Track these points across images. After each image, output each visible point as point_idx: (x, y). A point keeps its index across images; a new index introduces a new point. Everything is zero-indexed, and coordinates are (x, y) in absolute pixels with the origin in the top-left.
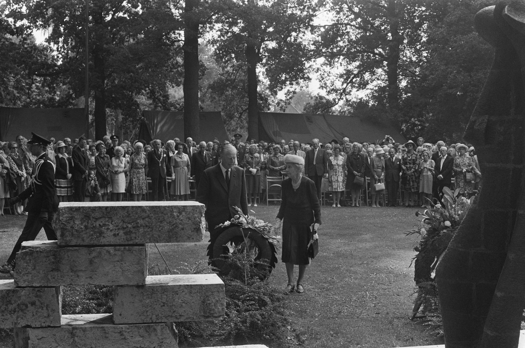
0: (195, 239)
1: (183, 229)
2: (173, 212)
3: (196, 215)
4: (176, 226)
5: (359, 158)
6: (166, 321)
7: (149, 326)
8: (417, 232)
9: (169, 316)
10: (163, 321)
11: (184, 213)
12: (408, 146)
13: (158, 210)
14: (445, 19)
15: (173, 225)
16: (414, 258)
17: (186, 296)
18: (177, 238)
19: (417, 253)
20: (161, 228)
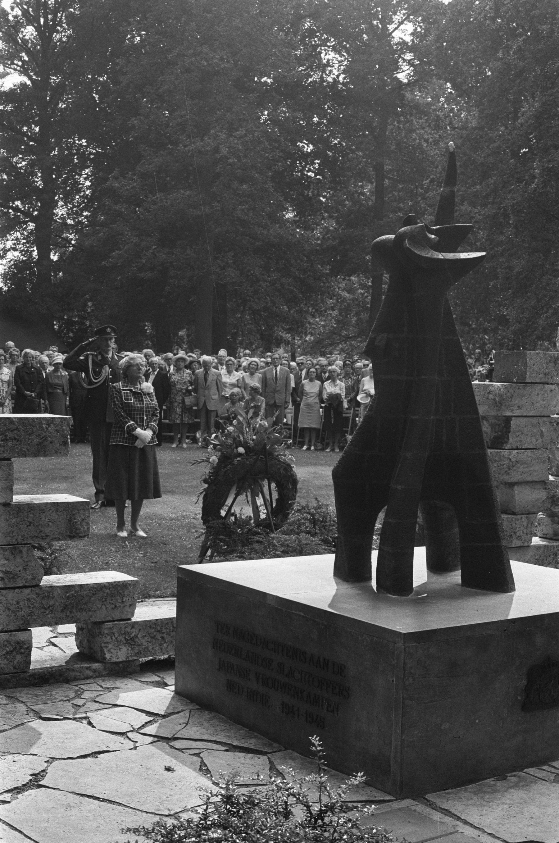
1: (51, 442)
2: (42, 424)
3: (64, 428)
4: (46, 439)
5: (33, 373)
6: (31, 542)
7: (15, 548)
8: (206, 461)
9: (35, 536)
11: (52, 426)
15: (43, 438)
16: (201, 493)
18: (45, 452)
19: (206, 486)
20: (30, 441)
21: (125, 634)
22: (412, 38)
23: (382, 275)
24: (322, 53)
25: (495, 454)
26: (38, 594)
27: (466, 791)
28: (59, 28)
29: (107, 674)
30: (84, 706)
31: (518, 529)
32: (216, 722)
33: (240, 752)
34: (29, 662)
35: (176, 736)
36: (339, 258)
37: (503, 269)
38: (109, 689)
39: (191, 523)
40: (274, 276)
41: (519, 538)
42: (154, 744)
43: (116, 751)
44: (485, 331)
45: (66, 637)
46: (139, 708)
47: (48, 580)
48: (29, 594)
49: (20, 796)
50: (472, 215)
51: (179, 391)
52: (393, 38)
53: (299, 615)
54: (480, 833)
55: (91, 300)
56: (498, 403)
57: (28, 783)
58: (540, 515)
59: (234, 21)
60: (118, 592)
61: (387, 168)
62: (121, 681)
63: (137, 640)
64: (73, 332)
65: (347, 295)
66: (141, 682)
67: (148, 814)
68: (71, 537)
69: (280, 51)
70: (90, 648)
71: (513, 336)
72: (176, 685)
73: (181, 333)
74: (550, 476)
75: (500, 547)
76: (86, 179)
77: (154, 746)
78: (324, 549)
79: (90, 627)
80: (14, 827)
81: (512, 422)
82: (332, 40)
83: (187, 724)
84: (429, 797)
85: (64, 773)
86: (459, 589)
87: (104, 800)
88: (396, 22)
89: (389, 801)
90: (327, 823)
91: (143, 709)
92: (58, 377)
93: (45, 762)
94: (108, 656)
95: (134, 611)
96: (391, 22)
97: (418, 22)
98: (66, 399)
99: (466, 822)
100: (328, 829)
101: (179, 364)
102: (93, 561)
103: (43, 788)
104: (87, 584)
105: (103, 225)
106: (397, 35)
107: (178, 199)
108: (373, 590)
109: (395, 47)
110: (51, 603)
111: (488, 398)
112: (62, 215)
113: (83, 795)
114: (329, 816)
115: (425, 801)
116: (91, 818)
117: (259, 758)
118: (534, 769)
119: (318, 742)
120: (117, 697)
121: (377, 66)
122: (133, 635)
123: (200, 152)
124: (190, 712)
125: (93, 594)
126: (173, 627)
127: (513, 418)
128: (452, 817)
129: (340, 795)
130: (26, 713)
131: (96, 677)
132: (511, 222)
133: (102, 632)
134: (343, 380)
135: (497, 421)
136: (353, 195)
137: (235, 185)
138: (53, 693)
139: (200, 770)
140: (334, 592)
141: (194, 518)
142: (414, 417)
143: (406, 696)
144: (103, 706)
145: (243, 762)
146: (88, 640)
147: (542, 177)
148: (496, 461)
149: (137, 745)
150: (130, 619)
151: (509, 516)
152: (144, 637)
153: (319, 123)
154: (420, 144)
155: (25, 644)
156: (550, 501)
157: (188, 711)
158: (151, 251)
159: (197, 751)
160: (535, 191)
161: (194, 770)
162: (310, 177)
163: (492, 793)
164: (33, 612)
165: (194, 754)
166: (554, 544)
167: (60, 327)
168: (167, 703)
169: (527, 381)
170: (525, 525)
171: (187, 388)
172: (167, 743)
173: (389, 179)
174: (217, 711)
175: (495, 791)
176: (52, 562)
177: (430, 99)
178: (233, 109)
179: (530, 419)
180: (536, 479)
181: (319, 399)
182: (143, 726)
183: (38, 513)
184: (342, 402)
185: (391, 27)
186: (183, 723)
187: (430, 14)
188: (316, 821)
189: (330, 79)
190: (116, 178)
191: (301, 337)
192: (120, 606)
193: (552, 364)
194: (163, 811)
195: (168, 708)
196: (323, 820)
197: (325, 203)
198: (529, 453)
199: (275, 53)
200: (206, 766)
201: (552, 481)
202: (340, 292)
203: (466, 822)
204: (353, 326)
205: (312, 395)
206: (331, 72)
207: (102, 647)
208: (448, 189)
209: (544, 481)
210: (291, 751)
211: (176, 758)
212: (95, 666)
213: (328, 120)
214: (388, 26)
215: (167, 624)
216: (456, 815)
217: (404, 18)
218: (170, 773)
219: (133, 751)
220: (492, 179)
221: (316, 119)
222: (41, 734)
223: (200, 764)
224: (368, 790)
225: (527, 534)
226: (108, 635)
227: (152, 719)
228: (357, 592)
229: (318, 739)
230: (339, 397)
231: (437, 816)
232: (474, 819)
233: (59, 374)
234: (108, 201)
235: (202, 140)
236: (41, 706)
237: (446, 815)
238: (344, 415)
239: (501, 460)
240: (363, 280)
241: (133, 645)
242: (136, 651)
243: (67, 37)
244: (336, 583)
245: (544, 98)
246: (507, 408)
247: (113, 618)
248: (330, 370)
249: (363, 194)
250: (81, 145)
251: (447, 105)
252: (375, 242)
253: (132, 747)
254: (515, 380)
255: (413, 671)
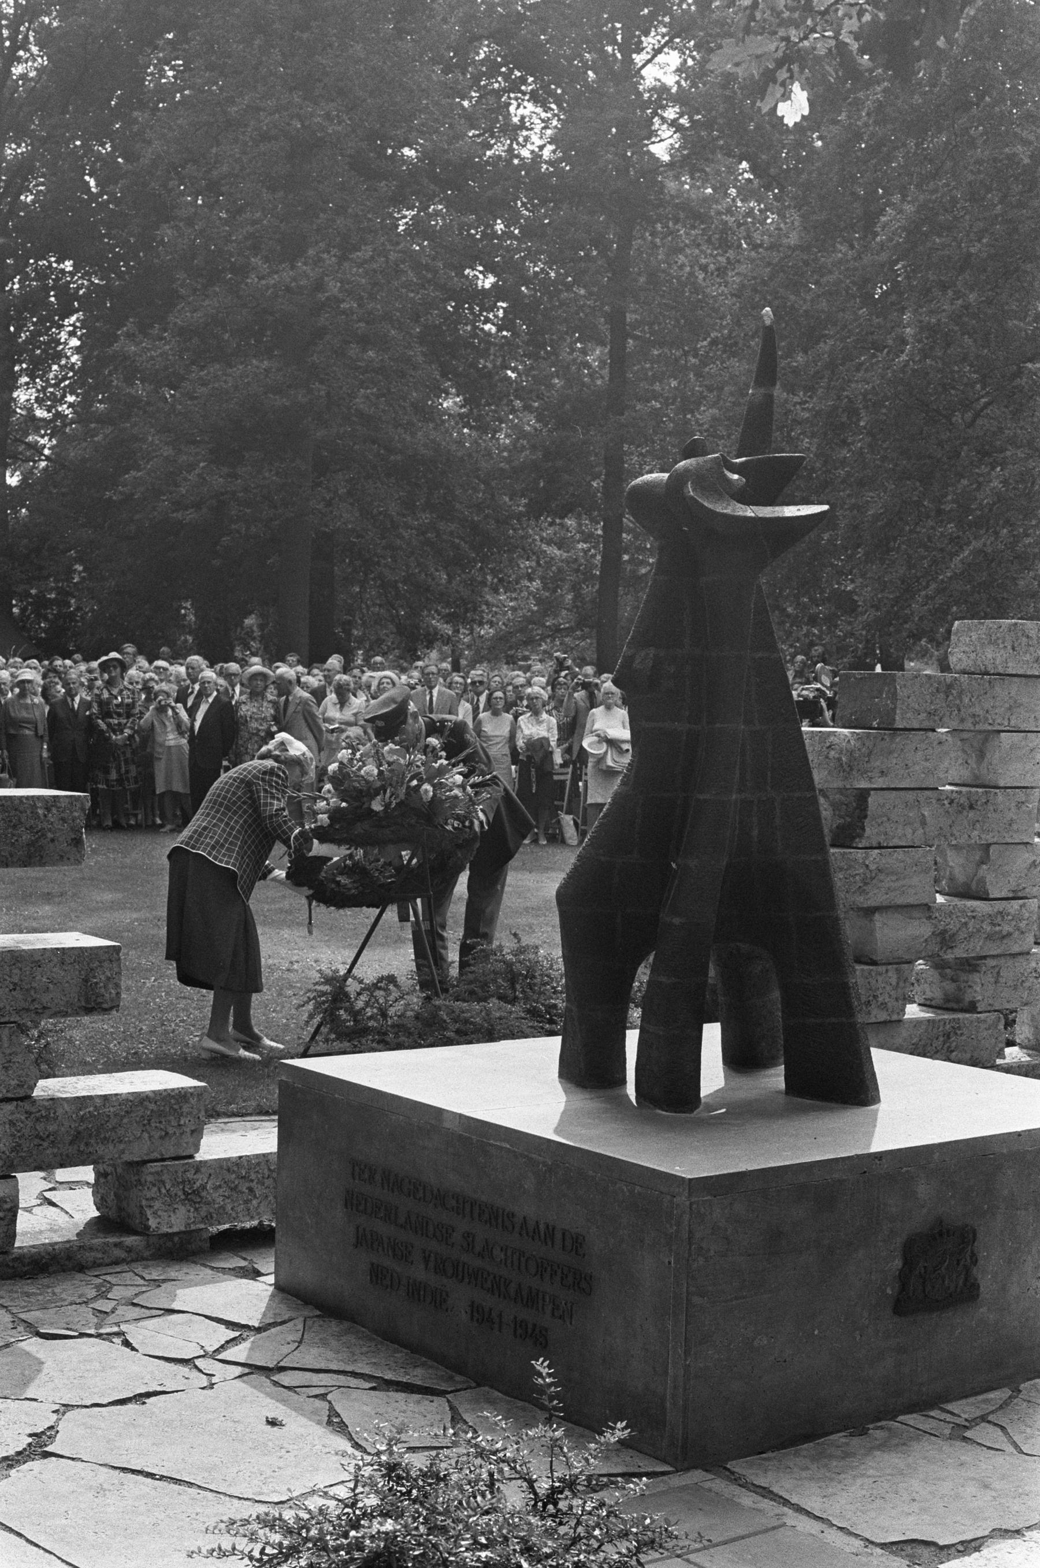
0: (72, 860)
1: (52, 840)
2: (37, 808)
3: (76, 814)
4: (43, 835)
6: (17, 1019)
10: (12, 1020)
11: (54, 810)
12: (109, 667)
13: (9, 803)
14: (171, 318)
17: (55, 970)
21: (183, 1182)
22: (677, 78)
23: (622, 516)
24: (510, 104)
25: (839, 857)
26: (29, 1113)
27: (797, 1454)
28: (21, 53)
29: (151, 1255)
30: (113, 1312)
31: (881, 991)
32: (351, 1338)
33: (397, 1391)
34: (13, 1236)
35: (282, 1364)
36: (542, 484)
37: (846, 510)
38: (157, 1283)
39: (284, 979)
40: (426, 517)
41: (883, 1006)
42: (245, 1378)
43: (177, 1391)
44: (813, 621)
45: (71, 1189)
46: (214, 1315)
47: (47, 1087)
48: (12, 1113)
49: (13, 1472)
50: (789, 406)
51: (253, 734)
52: (643, 78)
53: (501, 1148)
54: (824, 1527)
55: (79, 560)
56: (845, 767)
57: (25, 1449)
58: (920, 965)
59: (352, 46)
60: (171, 1107)
61: (630, 317)
62: (177, 1267)
63: (204, 1194)
64: (46, 619)
65: (557, 552)
66: (213, 1268)
67: (242, 1501)
68: (89, 1011)
69: (437, 104)
70: (120, 1209)
71: (864, 633)
72: (276, 1273)
73: (248, 622)
74: (937, 895)
75: (853, 1025)
76: (72, 334)
77: (244, 1382)
78: (532, 1027)
79: (119, 1170)
80: (7, 1527)
81: (870, 799)
82: (531, 79)
83: (300, 1342)
84: (734, 1465)
85: (88, 1431)
86: (782, 1099)
87: (162, 1478)
88: (649, 49)
89: (663, 1474)
90: (565, 1509)
91: (221, 1316)
92: (26, 707)
93: (53, 1412)
94: (152, 1223)
95: (199, 1142)
96: (639, 50)
97: (689, 48)
98: (42, 748)
99: (799, 1509)
100: (565, 1521)
101: (256, 686)
102: (109, 1049)
103: (53, 1459)
104: (116, 1095)
105: (103, 420)
106: (651, 76)
107: (247, 376)
108: (631, 1102)
109: (646, 95)
110: (51, 1128)
111: (827, 757)
112: (28, 400)
113: (124, 1470)
114: (566, 1498)
115: (727, 1473)
116: (143, 1508)
117: (432, 1401)
118: (915, 1415)
119: (547, 1370)
120: (173, 1297)
121: (614, 130)
122: (198, 1184)
123: (288, 289)
124: (305, 1321)
125: (127, 1112)
126: (269, 1170)
127: (872, 792)
128: (775, 1500)
129: (587, 1460)
130: (11, 1326)
131: (133, 1261)
132: (862, 424)
133: (143, 1180)
134: (554, 712)
135: (843, 798)
136: (568, 367)
137: (353, 350)
138: (57, 1290)
139: (329, 1423)
140: (562, 1107)
141: (288, 970)
142: (701, 797)
143: (692, 1289)
144: (148, 1313)
145: (405, 1407)
146: (116, 1195)
147: (919, 341)
148: (841, 869)
149: (214, 1380)
150: (191, 1157)
151: (866, 967)
152: (216, 1188)
153: (507, 235)
154: (691, 274)
155: (6, 1202)
156: (938, 939)
157: (302, 1319)
158: (196, 472)
159: (322, 1391)
160: (905, 366)
161: (319, 1423)
162: (489, 334)
163: (843, 1458)
164: (20, 1145)
165: (316, 1396)
166: (946, 1017)
167: (23, 610)
168: (263, 1306)
169: (896, 726)
170: (894, 983)
171: (269, 728)
172: (268, 1377)
173: (636, 338)
174: (354, 1321)
175: (846, 1455)
176: (40, 1054)
177: (709, 191)
178: (350, 210)
179: (902, 793)
180: (911, 900)
181: (510, 747)
182: (222, 1347)
183: (28, 968)
184: (551, 753)
185: (639, 59)
186: (294, 1341)
187: (711, 35)
188: (545, 1506)
189: (525, 153)
190: (129, 336)
191: (472, 630)
192: (175, 1133)
193: (942, 695)
194: (268, 1495)
195: (264, 1315)
196: (555, 1504)
197: (516, 381)
198: (900, 854)
199: (427, 107)
200: (339, 1416)
201: (942, 904)
202: (544, 547)
203: (799, 1509)
204: (568, 610)
205: (498, 740)
206: (527, 139)
207: (142, 1207)
208: (762, 390)
209: (926, 905)
210: (487, 1388)
211: (284, 1401)
212: (130, 1240)
213: (522, 229)
214: (634, 56)
215: (258, 1164)
216: (781, 1497)
217: (663, 42)
218: (276, 1429)
219: (208, 1392)
220: (825, 342)
221: (500, 227)
222: (43, 1363)
223: (327, 1413)
224: (627, 1455)
225: (897, 999)
226: (154, 1185)
227: (237, 1334)
228: (603, 1105)
229: (546, 1363)
230: (545, 744)
231: (748, 1499)
232: (813, 1504)
233: (29, 701)
234: (117, 379)
235: (293, 267)
236: (38, 1314)
237: (763, 1496)
238: (556, 778)
239: (850, 867)
240: (587, 525)
241: (199, 1203)
242: (203, 1214)
243: (36, 69)
244: (565, 1092)
245: (922, 197)
246: (862, 774)
247: (162, 1155)
248: (529, 694)
249: (587, 365)
250: (63, 271)
251: (742, 201)
252: (634, 487)
253: (205, 1385)
254: (875, 724)
255: (704, 1245)
